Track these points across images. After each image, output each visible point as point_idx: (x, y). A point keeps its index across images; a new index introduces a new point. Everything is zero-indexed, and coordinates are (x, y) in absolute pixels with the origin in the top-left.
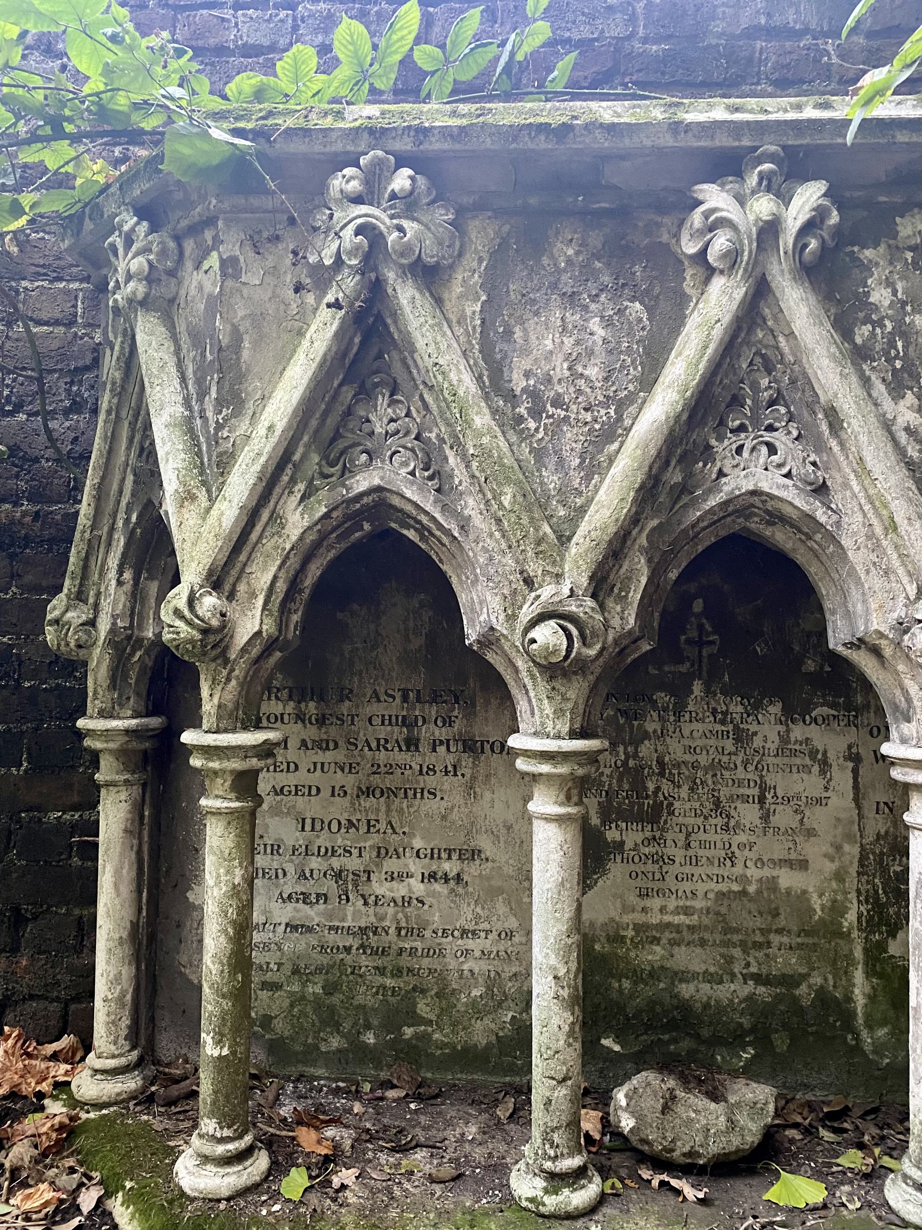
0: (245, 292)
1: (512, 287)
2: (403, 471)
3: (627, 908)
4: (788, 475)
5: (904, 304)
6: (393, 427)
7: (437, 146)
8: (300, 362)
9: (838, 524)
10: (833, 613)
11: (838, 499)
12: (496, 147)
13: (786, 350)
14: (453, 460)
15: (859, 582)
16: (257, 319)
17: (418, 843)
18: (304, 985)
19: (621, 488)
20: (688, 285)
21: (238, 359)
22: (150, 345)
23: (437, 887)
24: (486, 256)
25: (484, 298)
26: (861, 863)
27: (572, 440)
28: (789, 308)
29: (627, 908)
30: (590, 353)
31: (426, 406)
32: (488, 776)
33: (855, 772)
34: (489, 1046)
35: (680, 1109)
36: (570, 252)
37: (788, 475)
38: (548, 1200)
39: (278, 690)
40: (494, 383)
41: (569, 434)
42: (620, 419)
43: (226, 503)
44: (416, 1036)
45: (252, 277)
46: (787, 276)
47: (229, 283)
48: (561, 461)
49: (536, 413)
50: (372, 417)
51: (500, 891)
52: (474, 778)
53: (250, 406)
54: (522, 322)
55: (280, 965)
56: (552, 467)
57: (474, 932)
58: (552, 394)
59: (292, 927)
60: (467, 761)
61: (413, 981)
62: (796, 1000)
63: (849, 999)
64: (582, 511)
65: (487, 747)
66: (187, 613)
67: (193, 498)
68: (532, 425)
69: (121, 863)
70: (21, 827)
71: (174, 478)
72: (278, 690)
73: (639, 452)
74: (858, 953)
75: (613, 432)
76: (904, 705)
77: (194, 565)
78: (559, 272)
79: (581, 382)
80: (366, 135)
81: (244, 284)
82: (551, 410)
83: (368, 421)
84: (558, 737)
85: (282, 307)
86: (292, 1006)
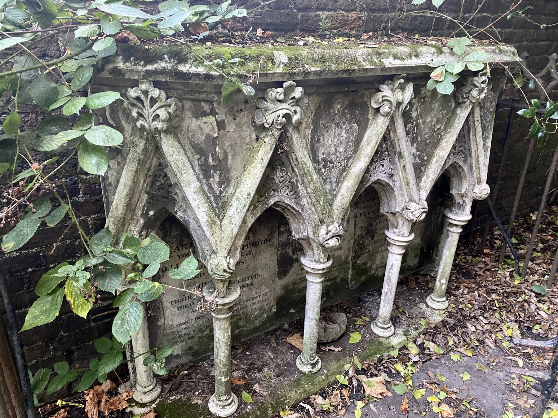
0: (228, 135)
1: (321, 122)
2: (285, 194)
3: (298, 275)
4: (385, 173)
5: (419, 116)
6: (282, 179)
7: (311, 78)
8: (258, 168)
9: (394, 185)
10: (384, 204)
11: (396, 178)
12: (330, 77)
13: (392, 136)
14: (300, 187)
15: (395, 199)
16: (233, 146)
17: (238, 279)
18: (203, 333)
19: (351, 191)
20: (370, 116)
21: (227, 164)
22: (174, 152)
23: (244, 289)
24: (313, 111)
25: (312, 128)
26: (354, 244)
27: (335, 173)
28: (398, 126)
29: (298, 275)
30: (341, 143)
31: (293, 171)
32: (260, 252)
33: (355, 221)
34: (260, 326)
35: (328, 330)
36: (339, 107)
37: (385, 173)
38: (313, 370)
39: (186, 245)
40: (315, 160)
41: (334, 171)
42: (347, 164)
43: (233, 225)
44: (239, 332)
45: (230, 128)
46: (400, 117)
47: (222, 132)
48: (331, 182)
49: (325, 167)
50: (275, 178)
51: (263, 283)
52: (256, 253)
53: (233, 183)
54: (323, 135)
55: (194, 331)
56: (328, 183)
57: (256, 297)
58: (330, 159)
59: (197, 318)
60: (254, 249)
61: (238, 317)
62: (336, 282)
63: (347, 277)
64: (335, 196)
65: (260, 242)
66: (228, 270)
67: (215, 223)
68: (323, 170)
69: (144, 329)
70: (63, 321)
71: (205, 216)
72: (186, 245)
73: (356, 179)
74: (351, 266)
75: (345, 169)
76: (396, 225)
77: (223, 250)
78: (335, 115)
79: (338, 154)
80: (288, 75)
81: (227, 131)
82: (329, 164)
83: (274, 179)
84: (325, 263)
85: (243, 140)
86: (199, 340)
